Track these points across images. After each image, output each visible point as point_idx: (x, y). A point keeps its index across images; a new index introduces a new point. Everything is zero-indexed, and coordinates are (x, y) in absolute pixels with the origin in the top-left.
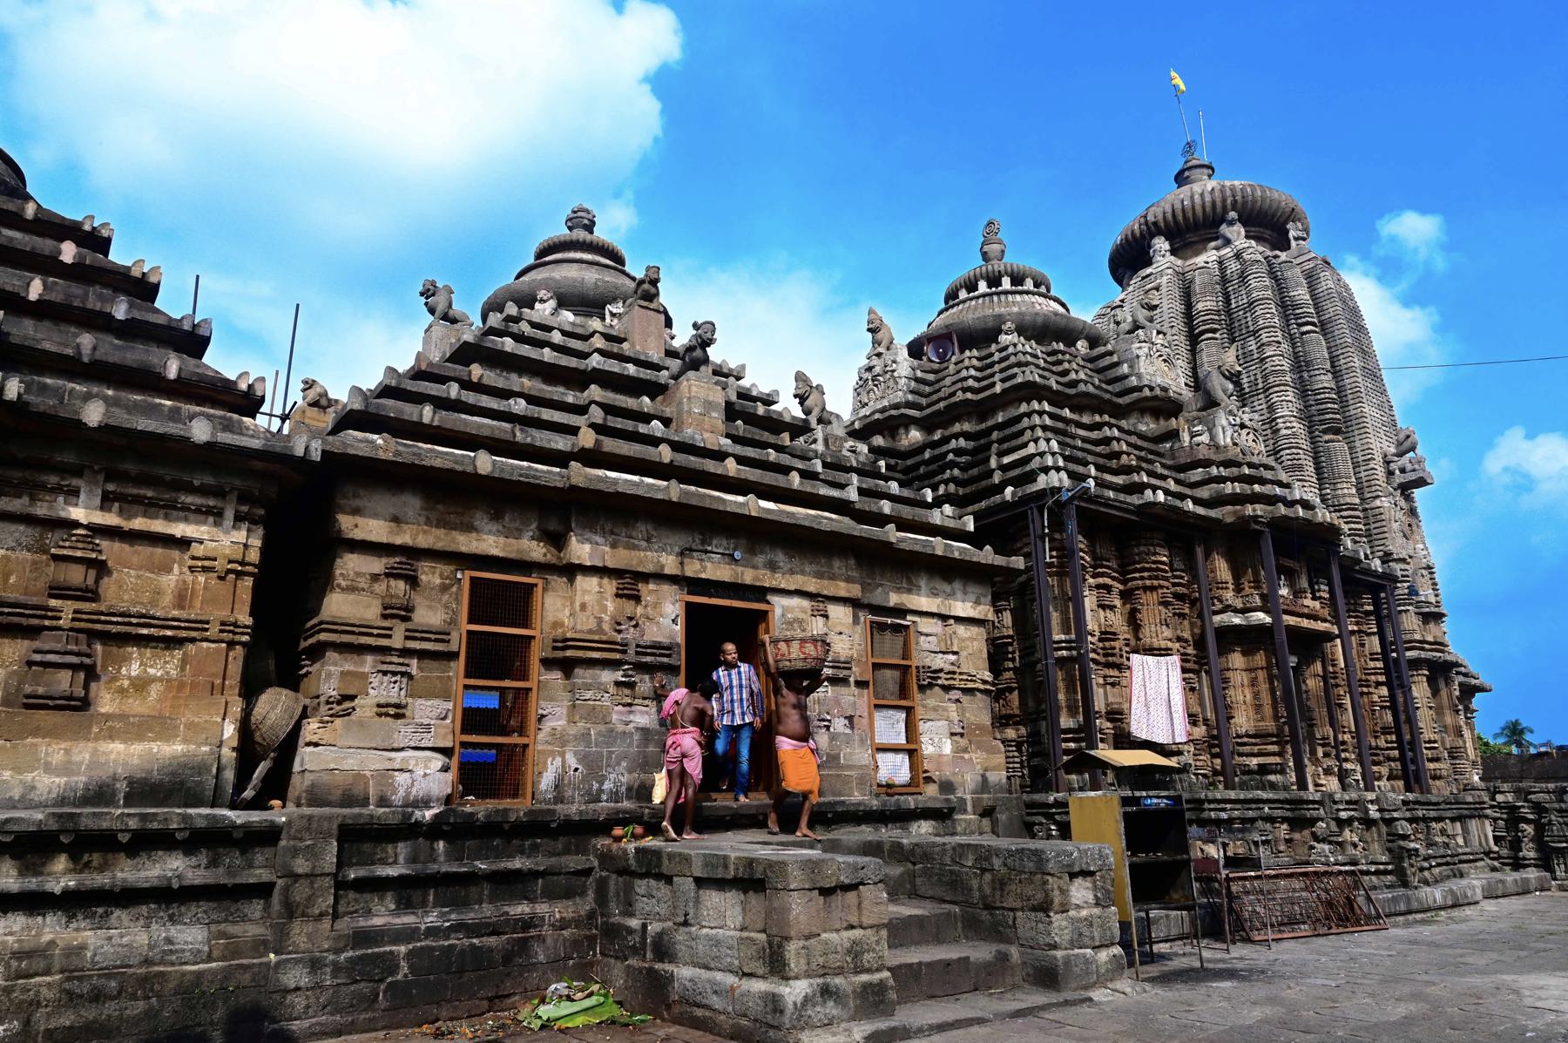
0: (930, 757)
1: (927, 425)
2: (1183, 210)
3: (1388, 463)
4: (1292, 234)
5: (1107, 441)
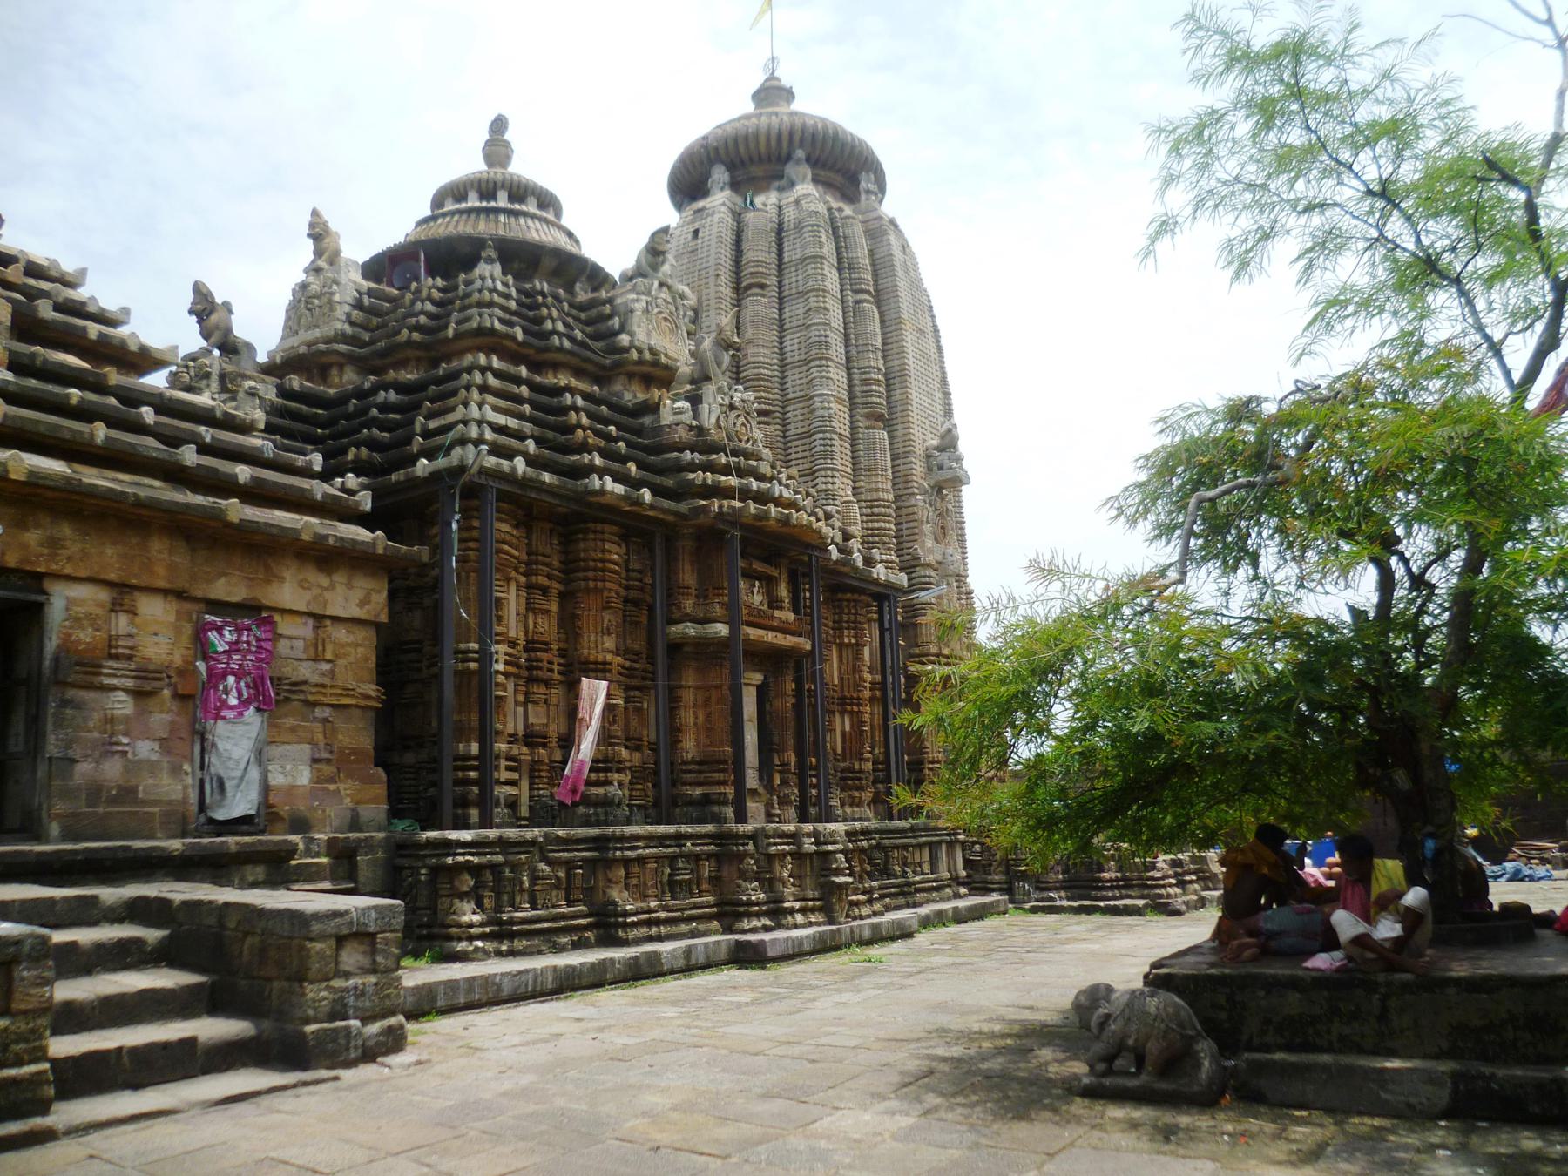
1: (364, 365)
2: (768, 139)
3: (929, 456)
4: (863, 185)
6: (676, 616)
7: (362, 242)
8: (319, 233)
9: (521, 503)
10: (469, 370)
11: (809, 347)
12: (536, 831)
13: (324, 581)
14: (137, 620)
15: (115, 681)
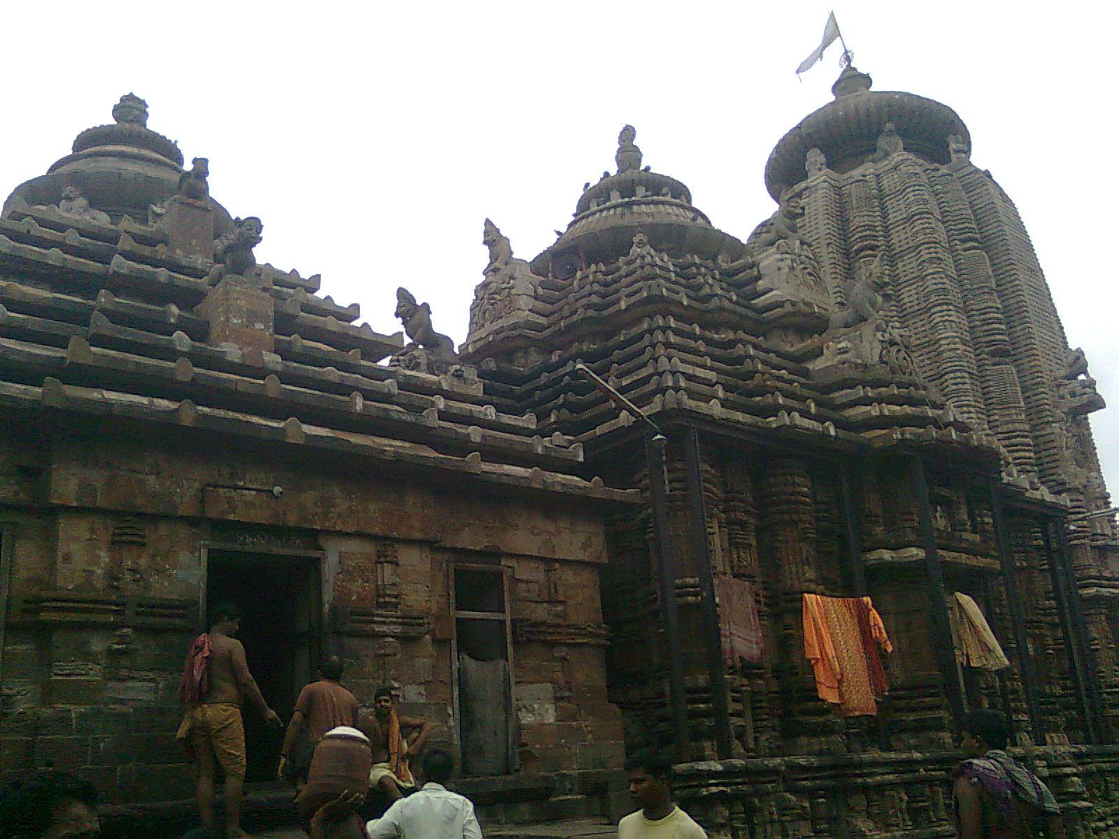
0: (530, 727)
4: (953, 146)
5: (740, 360)
6: (867, 544)
7: (531, 241)
8: (494, 238)
9: (721, 444)
10: (651, 331)
11: (927, 296)
12: (778, 760)
13: (551, 528)
14: (399, 571)
15: (384, 628)
